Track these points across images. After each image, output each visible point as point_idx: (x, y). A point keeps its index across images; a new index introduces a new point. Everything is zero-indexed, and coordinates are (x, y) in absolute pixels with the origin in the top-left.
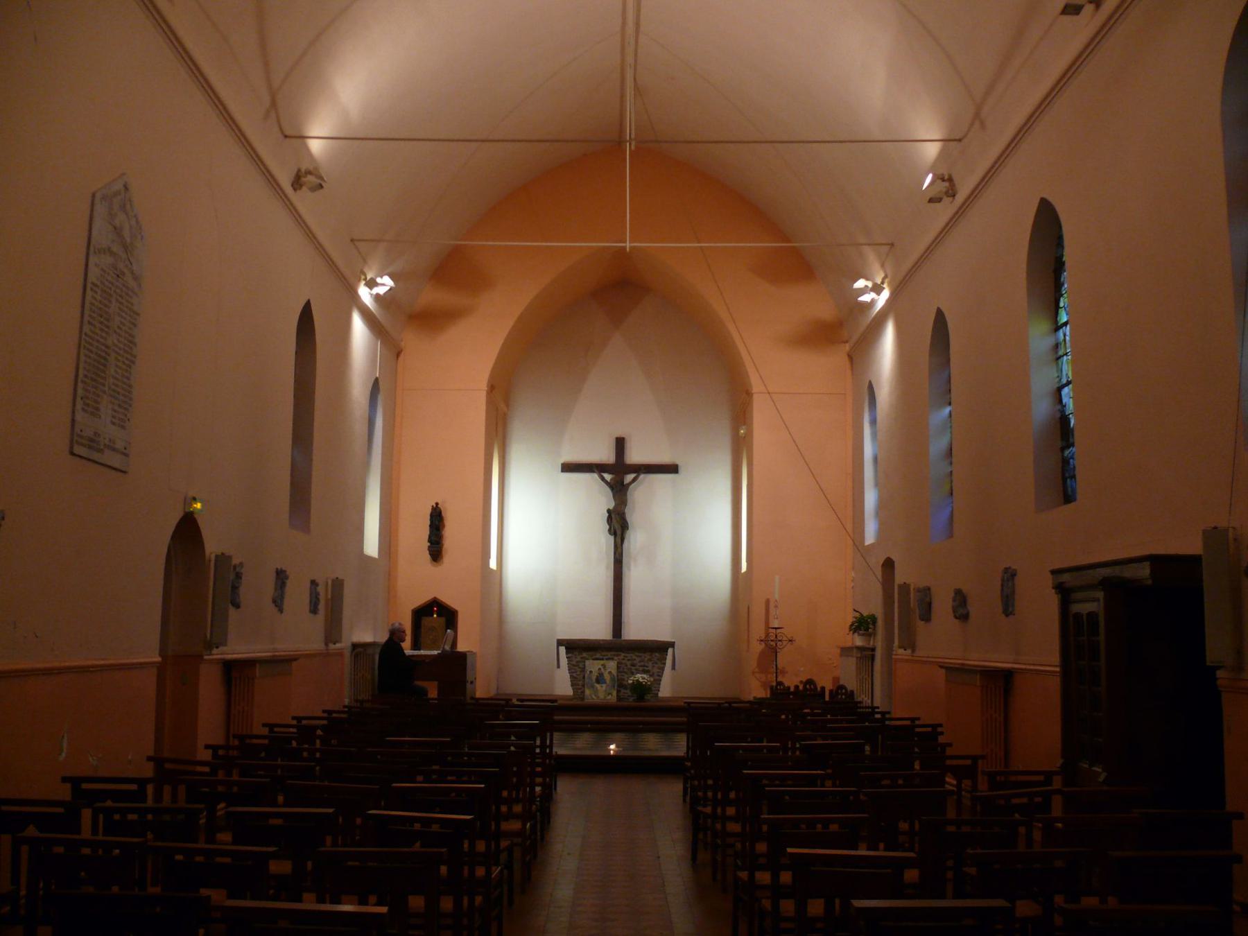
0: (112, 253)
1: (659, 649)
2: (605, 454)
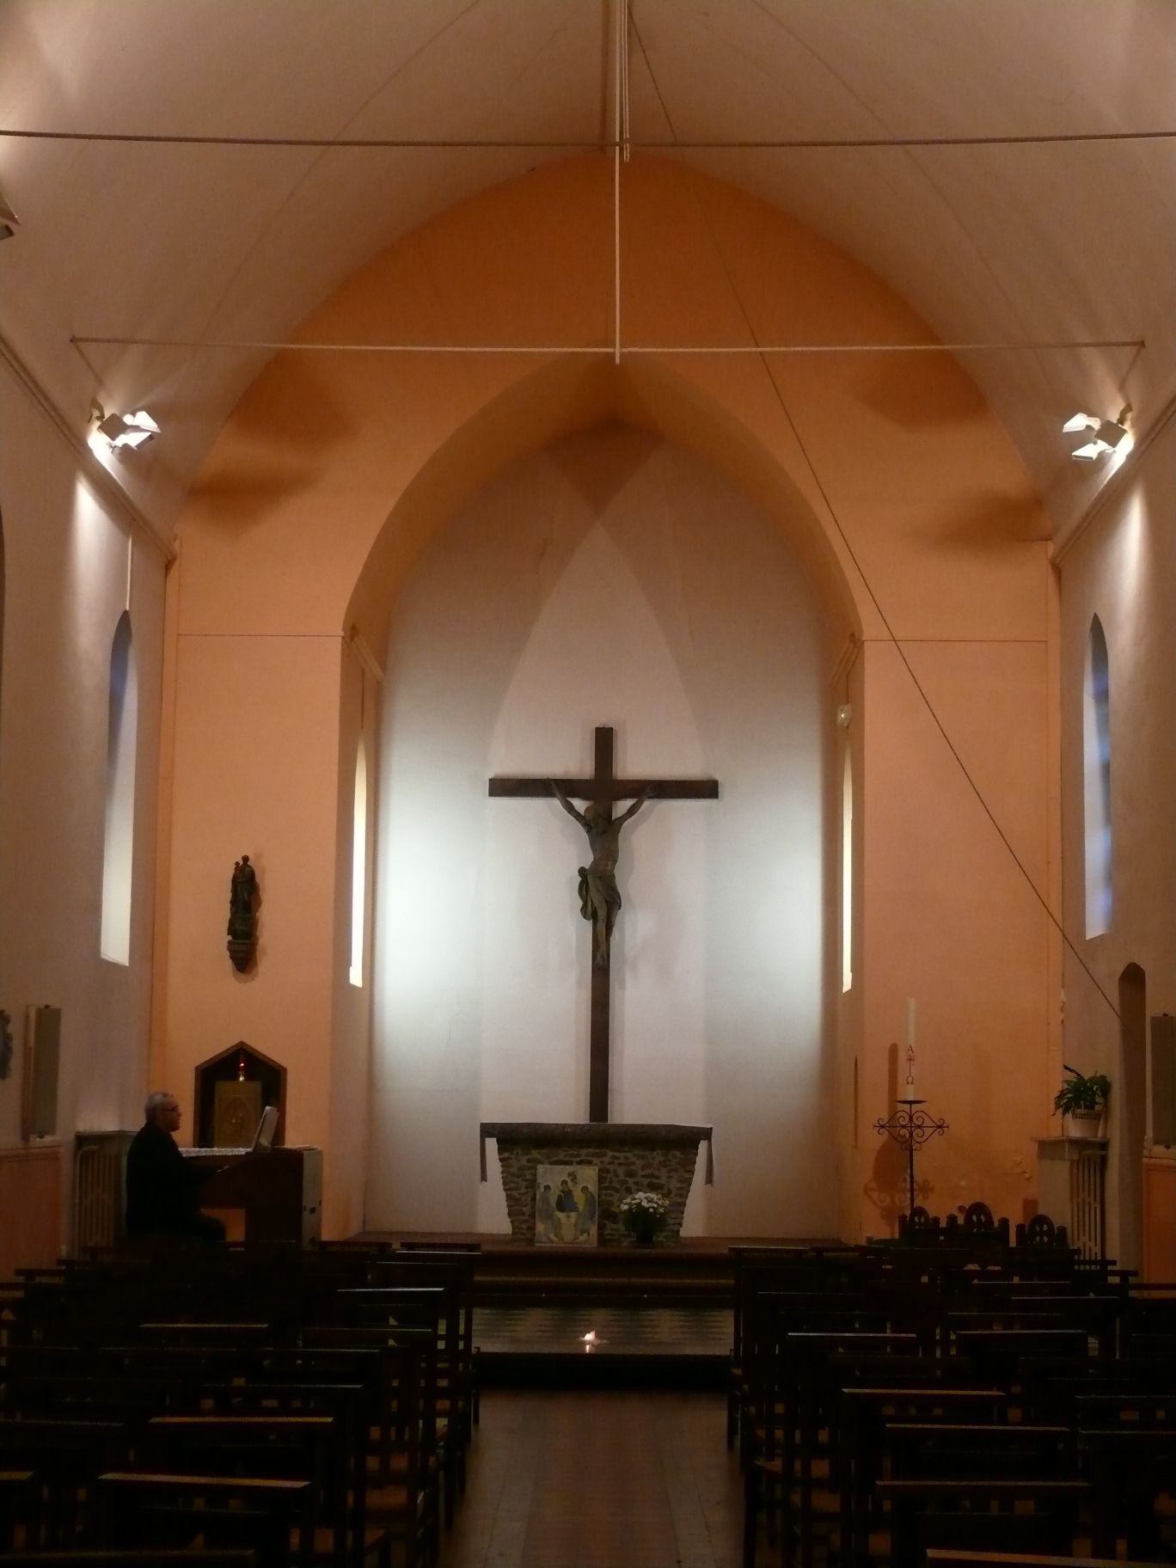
1: (679, 1143)
2: (576, 762)
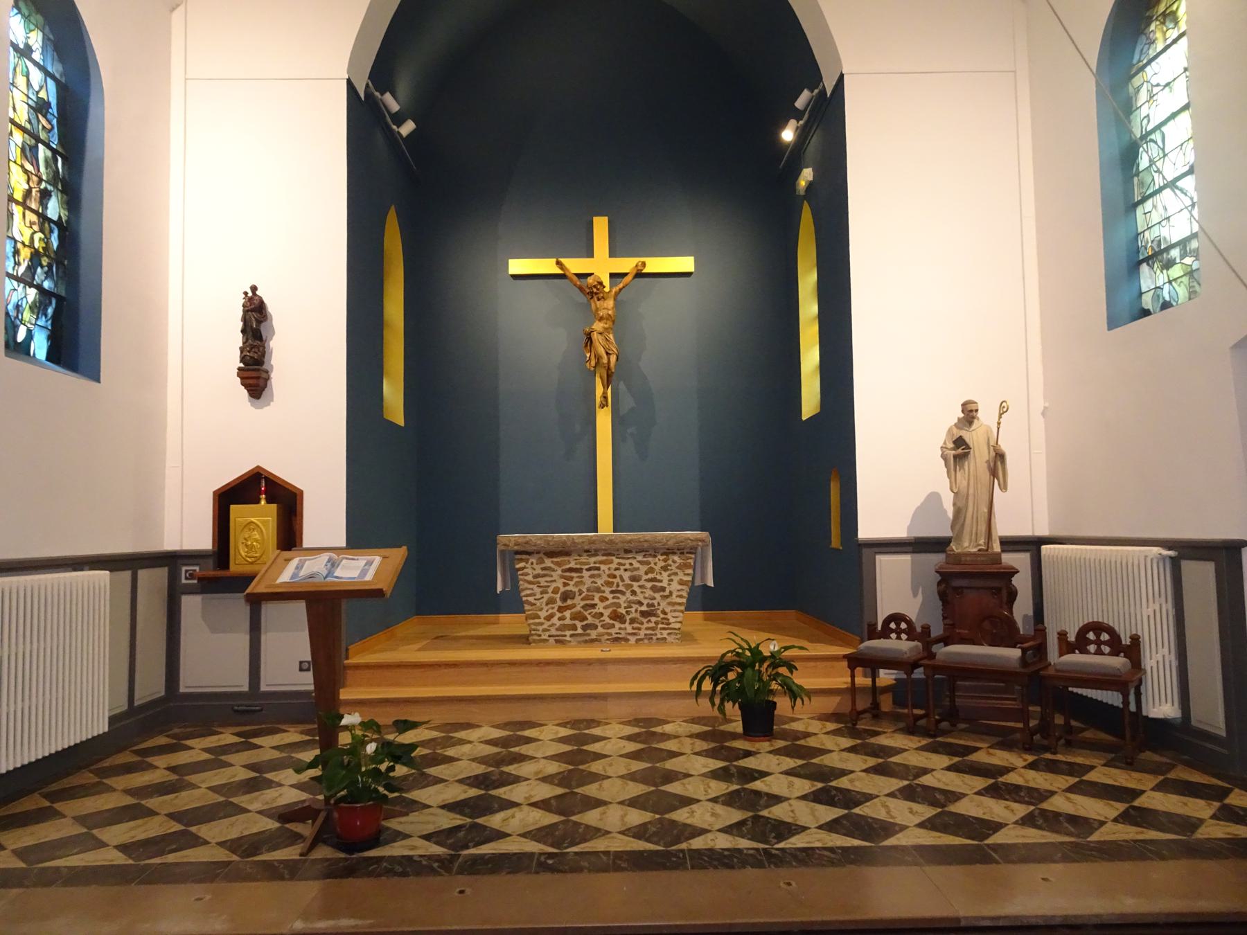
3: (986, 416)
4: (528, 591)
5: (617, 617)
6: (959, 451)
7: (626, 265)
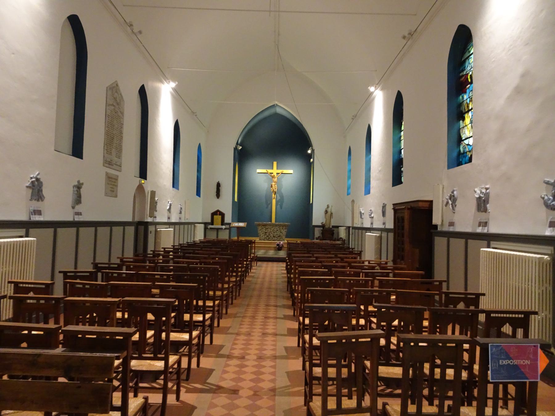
0: (113, 105)
3: (330, 206)
4: (259, 232)
5: (274, 237)
6: (326, 212)
7: (279, 171)
